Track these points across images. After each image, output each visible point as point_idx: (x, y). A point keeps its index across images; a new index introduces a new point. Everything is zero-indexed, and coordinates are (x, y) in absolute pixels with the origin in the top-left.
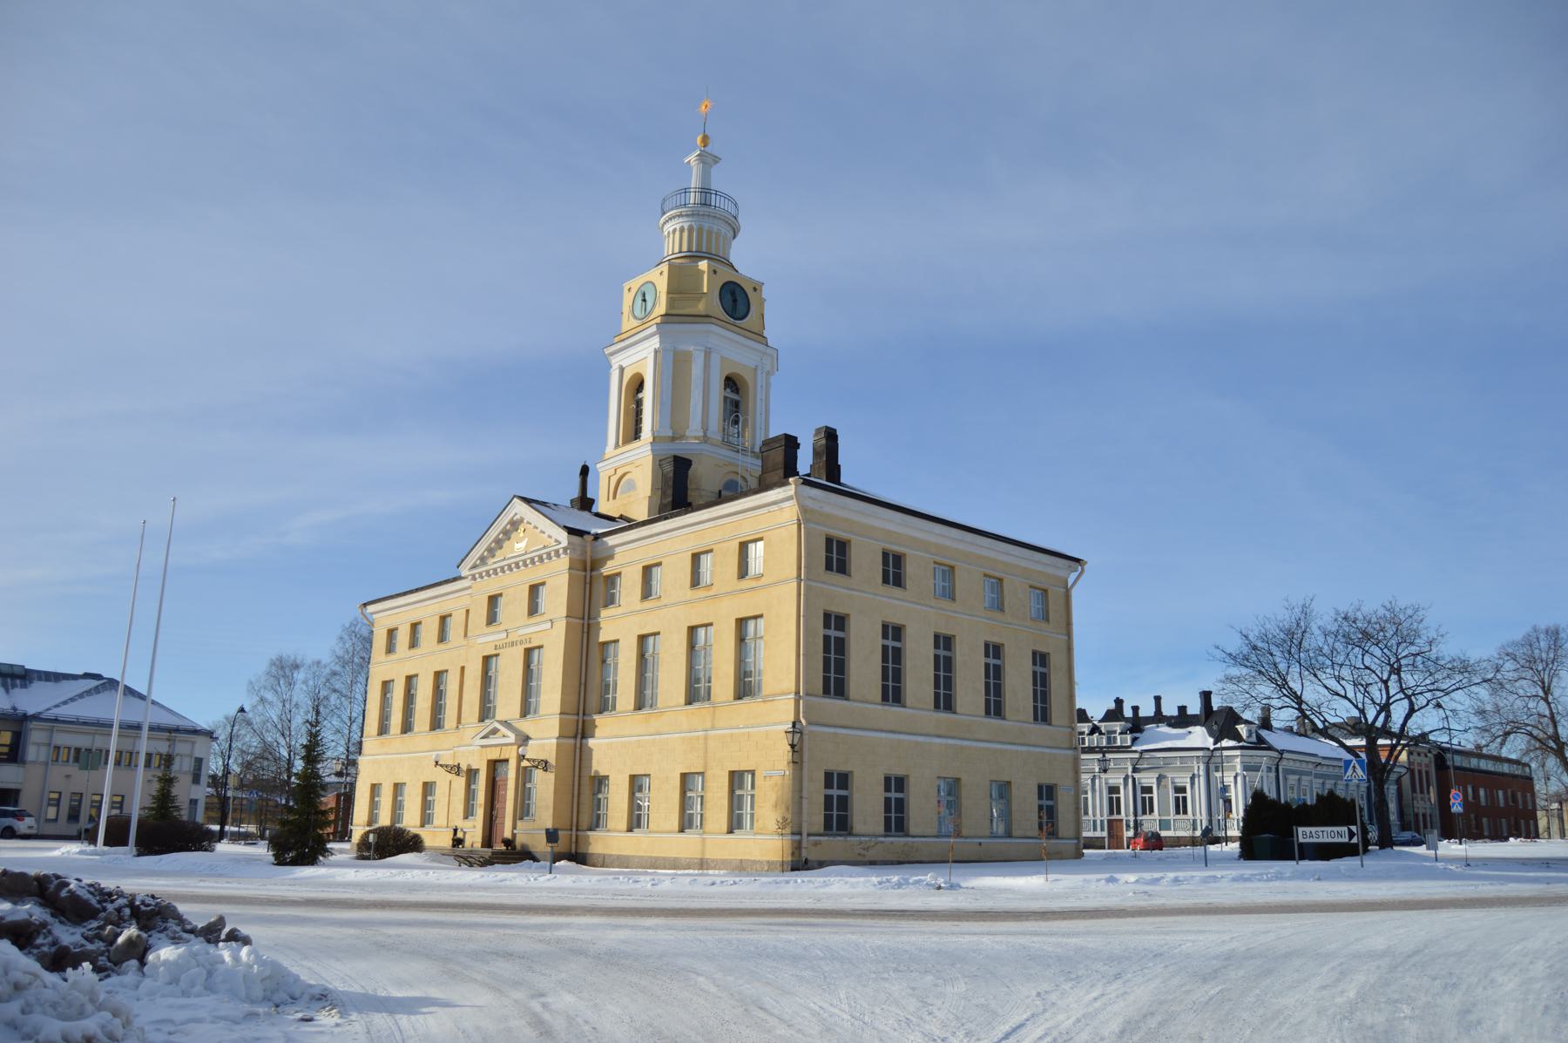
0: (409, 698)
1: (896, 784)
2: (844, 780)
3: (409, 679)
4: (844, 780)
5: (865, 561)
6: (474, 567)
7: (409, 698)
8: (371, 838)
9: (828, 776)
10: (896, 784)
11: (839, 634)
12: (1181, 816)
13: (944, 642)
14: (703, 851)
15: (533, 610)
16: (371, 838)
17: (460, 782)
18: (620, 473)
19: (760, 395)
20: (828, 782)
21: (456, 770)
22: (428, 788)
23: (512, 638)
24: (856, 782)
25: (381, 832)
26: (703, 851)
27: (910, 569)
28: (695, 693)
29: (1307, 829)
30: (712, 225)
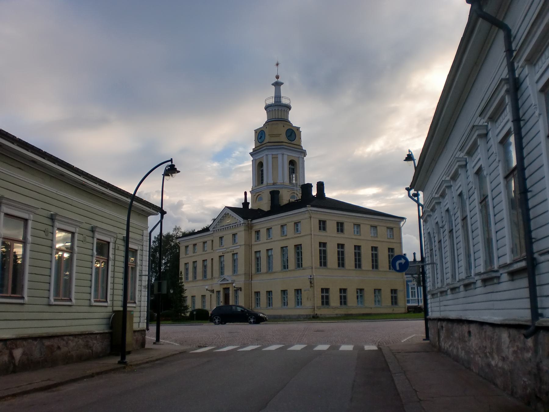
0: (195, 268)
1: (343, 291)
2: (327, 290)
3: (195, 262)
4: (327, 290)
5: (331, 226)
6: (214, 228)
7: (195, 268)
8: (195, 313)
9: (322, 289)
10: (343, 291)
11: (324, 249)
12: (413, 298)
13: (358, 248)
14: (528, 309)
15: (234, 241)
16: (195, 313)
17: (214, 295)
18: (257, 194)
19: (301, 166)
20: (322, 292)
21: (212, 291)
22: (203, 296)
23: (228, 250)
24: (331, 291)
25: (199, 311)
26: (528, 309)
27: (346, 227)
28: (285, 266)
29: (136, 320)
30: (278, 111)
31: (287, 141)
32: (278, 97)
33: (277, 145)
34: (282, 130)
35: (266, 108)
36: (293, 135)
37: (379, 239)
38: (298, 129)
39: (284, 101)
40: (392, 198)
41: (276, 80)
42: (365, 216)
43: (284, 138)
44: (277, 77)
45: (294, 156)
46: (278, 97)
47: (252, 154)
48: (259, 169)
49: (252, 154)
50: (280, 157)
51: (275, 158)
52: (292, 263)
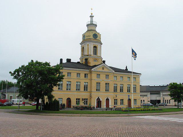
5: (82, 75)
31: (93, 38)
32: (92, 21)
33: (89, 40)
34: (91, 34)
35: (87, 26)
36: (96, 36)
37: (136, 82)
38: (98, 33)
39: (94, 23)
40: (66, 105)
41: (91, 15)
42: (117, 73)
43: (92, 37)
44: (92, 14)
45: (96, 44)
46: (92, 21)
47: (81, 44)
48: (83, 49)
49: (81, 44)
50: (90, 45)
51: (88, 45)
52: (167, 101)
